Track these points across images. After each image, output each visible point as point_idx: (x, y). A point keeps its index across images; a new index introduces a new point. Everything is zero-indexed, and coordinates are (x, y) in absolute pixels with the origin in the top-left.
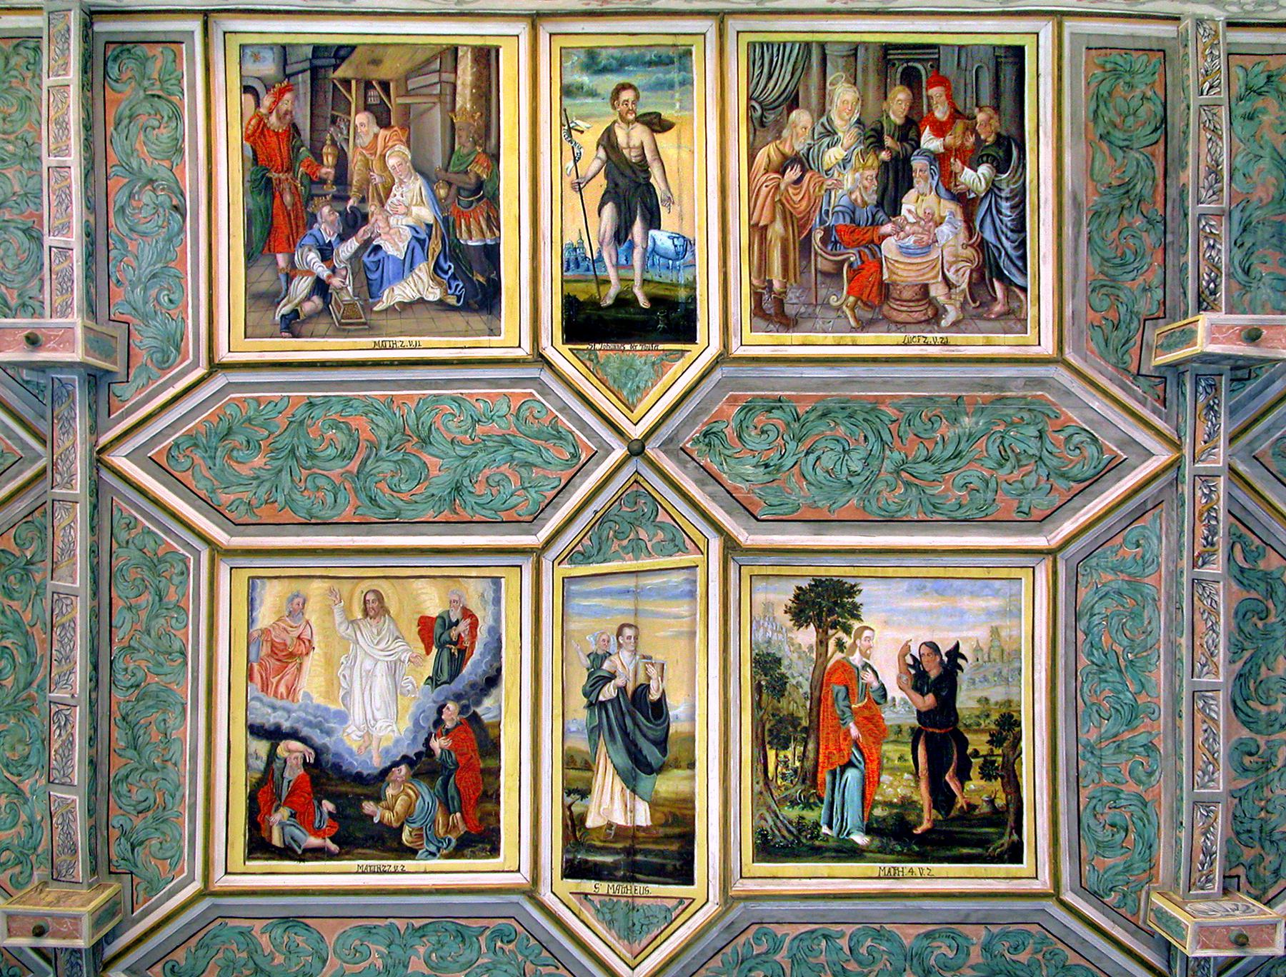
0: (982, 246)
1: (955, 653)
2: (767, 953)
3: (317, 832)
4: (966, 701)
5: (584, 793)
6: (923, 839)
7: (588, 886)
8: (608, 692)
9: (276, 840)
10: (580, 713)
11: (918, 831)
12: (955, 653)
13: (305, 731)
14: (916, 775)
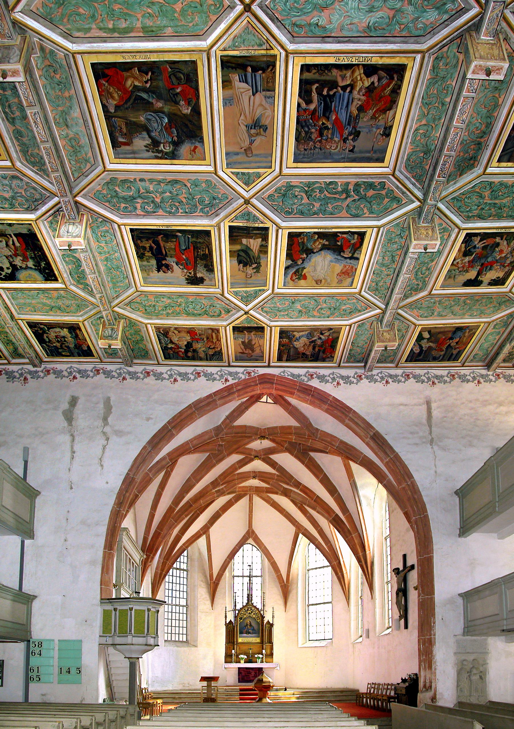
0: (167, 337)
1: (158, 271)
2: (205, 208)
3: (344, 238)
4: (154, 262)
5: (261, 246)
6: (160, 234)
7: (261, 225)
8: (254, 266)
9: (356, 236)
10: (262, 262)
11: (162, 236)
12: (158, 271)
13: (342, 259)
14: (165, 248)
